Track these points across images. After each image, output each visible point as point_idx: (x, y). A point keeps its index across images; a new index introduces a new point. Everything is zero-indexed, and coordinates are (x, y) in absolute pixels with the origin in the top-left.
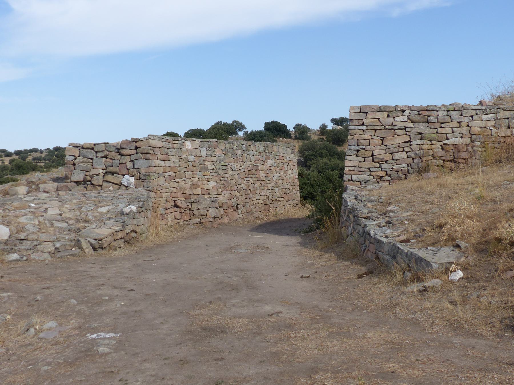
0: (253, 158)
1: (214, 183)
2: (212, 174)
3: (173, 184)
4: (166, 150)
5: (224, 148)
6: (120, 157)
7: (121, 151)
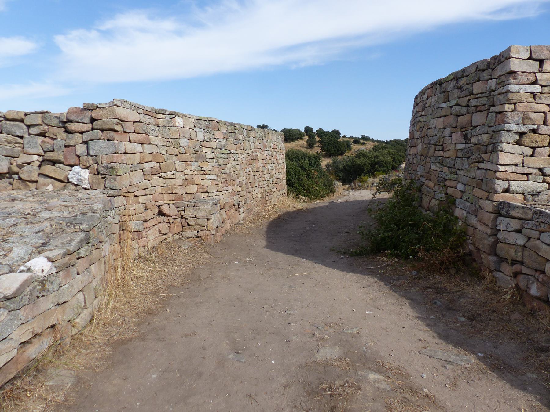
0: (253, 145)
1: (213, 177)
2: (210, 165)
3: (156, 180)
4: (145, 127)
5: (225, 130)
6: (65, 134)
7: (68, 125)
